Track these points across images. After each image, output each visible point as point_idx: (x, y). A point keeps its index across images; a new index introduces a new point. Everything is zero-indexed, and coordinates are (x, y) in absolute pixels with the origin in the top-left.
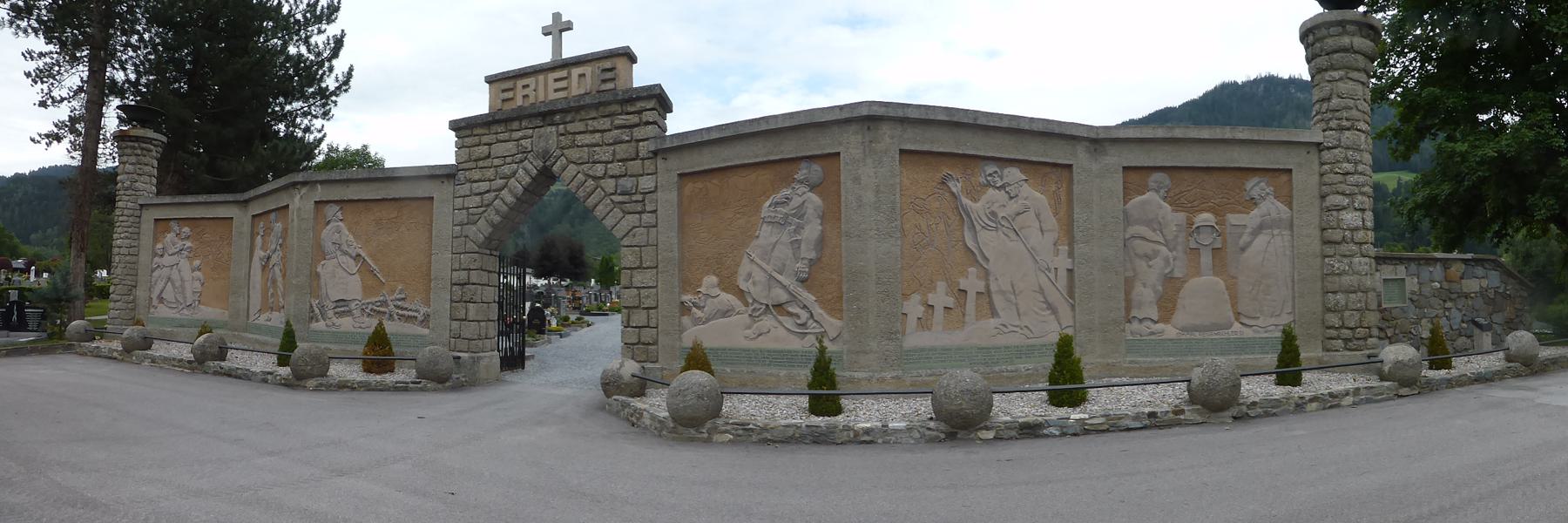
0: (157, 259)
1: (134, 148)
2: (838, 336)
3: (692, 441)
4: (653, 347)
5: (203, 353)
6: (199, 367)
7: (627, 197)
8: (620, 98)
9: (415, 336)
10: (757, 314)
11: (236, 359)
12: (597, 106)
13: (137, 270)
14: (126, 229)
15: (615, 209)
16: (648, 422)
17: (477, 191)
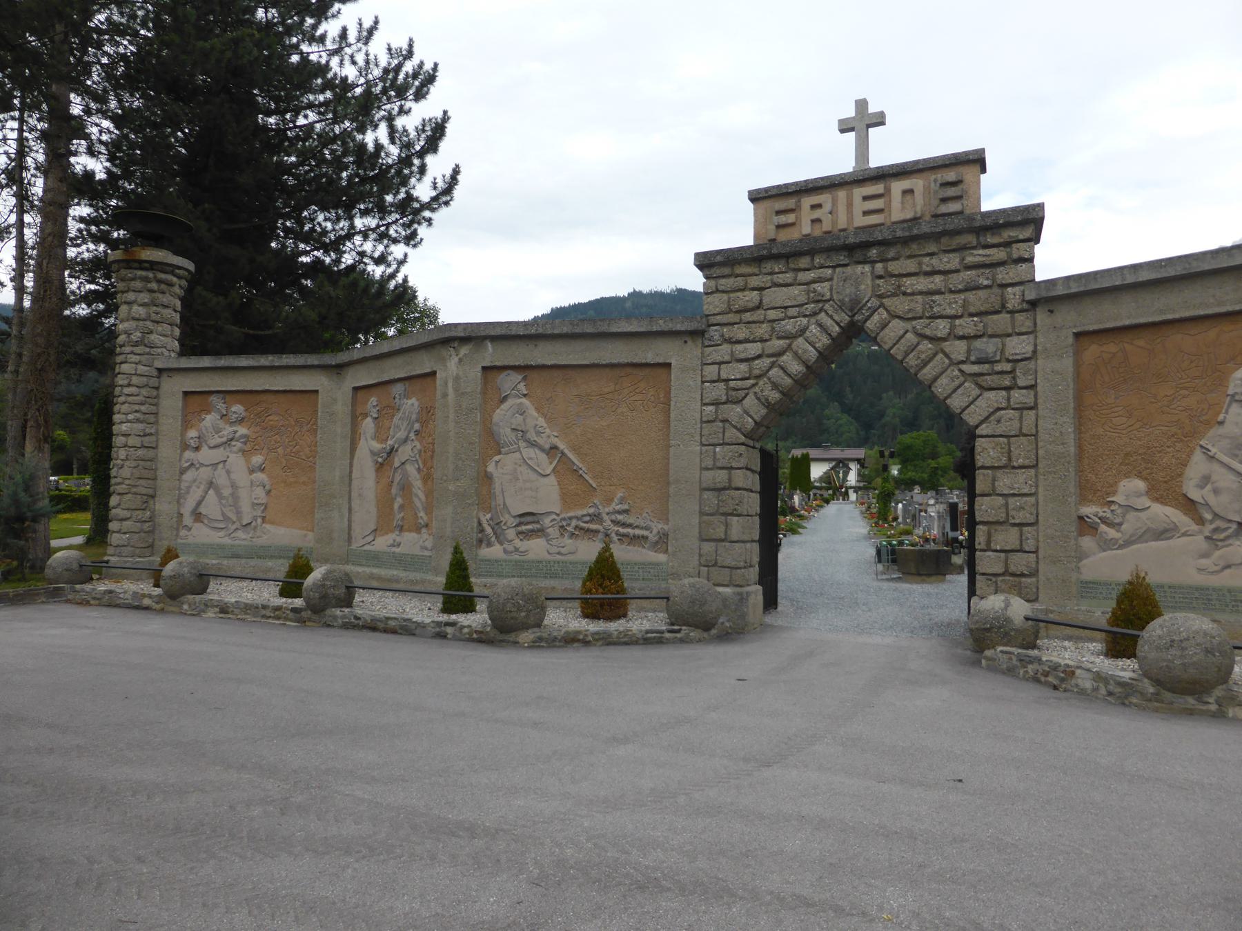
0: (188, 454)
1: (146, 280)
3: (1191, 714)
4: (1029, 580)
5: (324, 597)
6: (315, 617)
7: (987, 366)
8: (977, 224)
9: (645, 565)
10: (1222, 536)
11: (369, 604)
12: (936, 236)
13: (156, 469)
14: (137, 407)
15: (966, 384)
16: (1088, 685)
17: (742, 356)
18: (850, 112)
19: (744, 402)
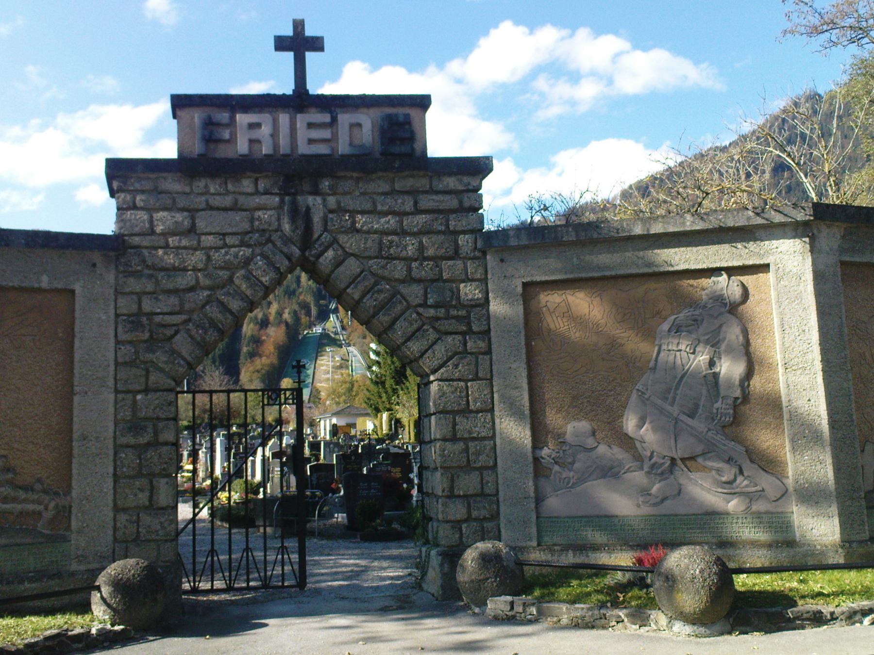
2: (783, 496)
18: (288, 31)
19: (174, 340)
